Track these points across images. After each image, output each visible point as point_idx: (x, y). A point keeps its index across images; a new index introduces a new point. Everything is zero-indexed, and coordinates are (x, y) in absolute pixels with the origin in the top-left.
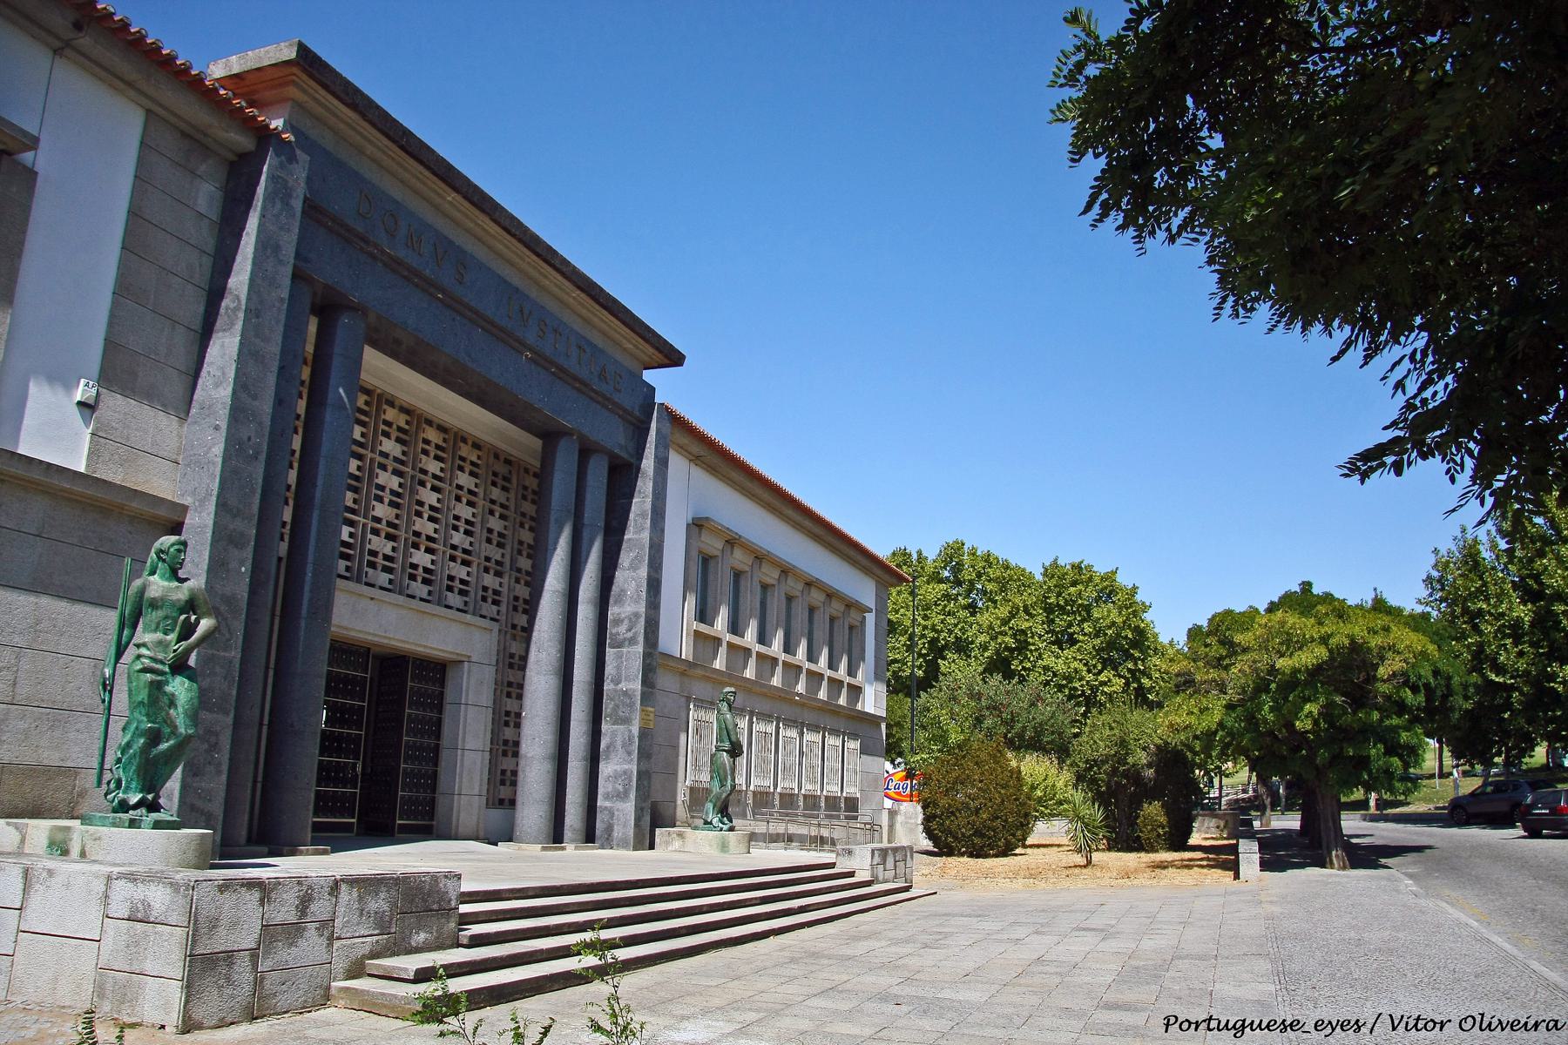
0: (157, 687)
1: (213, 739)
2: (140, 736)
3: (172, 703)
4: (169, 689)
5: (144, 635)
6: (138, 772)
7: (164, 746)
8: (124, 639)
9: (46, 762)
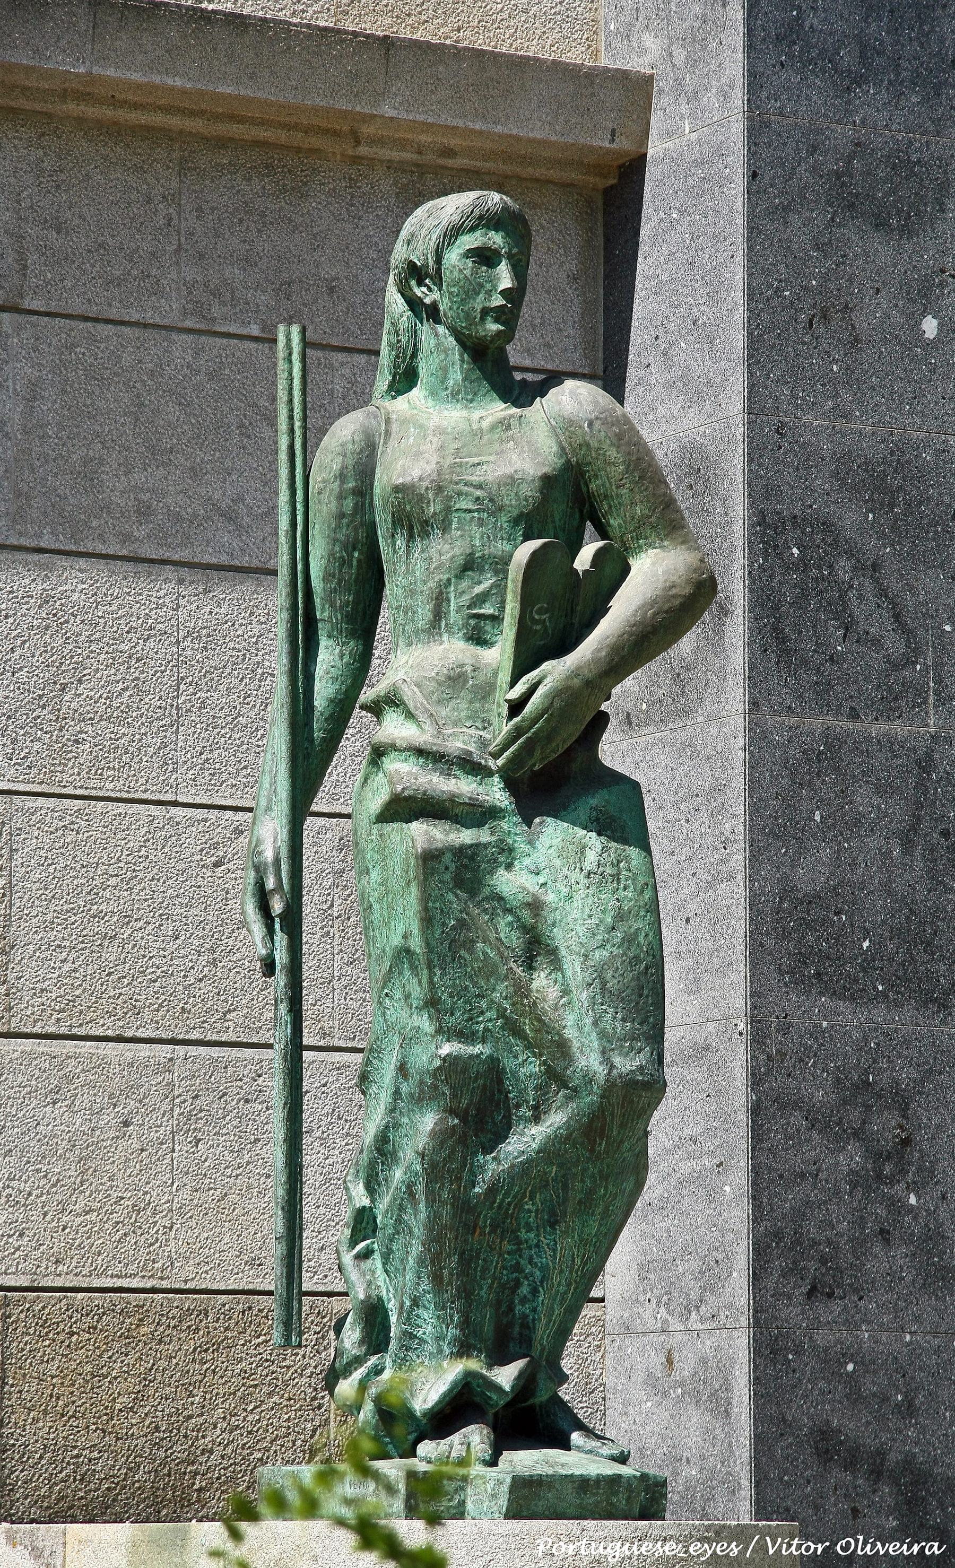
0: (458, 877)
1: (885, 1126)
2: (420, 1100)
3: (536, 948)
4: (511, 882)
5: (408, 661)
6: (433, 1261)
7: (525, 1140)
8: (324, 691)
9: (185, 1274)
